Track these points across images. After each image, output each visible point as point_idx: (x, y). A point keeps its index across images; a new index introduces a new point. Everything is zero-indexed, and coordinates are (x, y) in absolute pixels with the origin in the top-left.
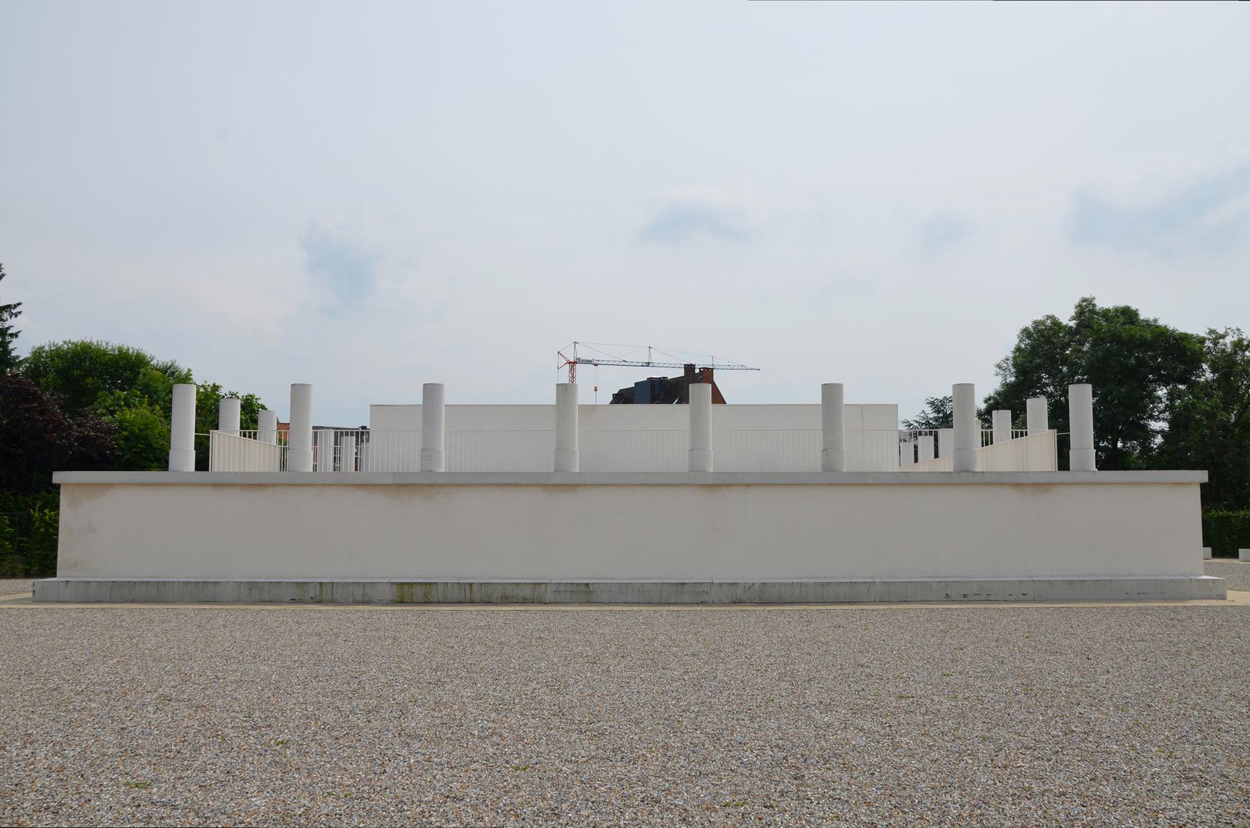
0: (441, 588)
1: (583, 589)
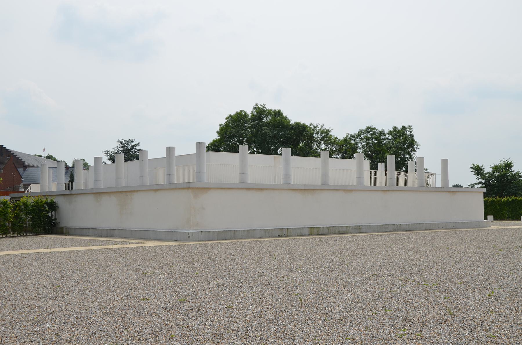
0: (322, 229)
1: (359, 227)
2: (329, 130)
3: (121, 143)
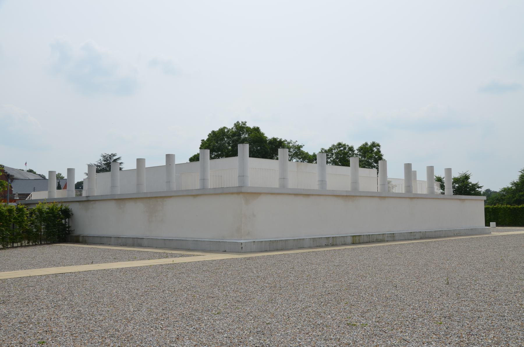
0: (362, 236)
1: (393, 235)
2: (301, 146)
3: (104, 157)
